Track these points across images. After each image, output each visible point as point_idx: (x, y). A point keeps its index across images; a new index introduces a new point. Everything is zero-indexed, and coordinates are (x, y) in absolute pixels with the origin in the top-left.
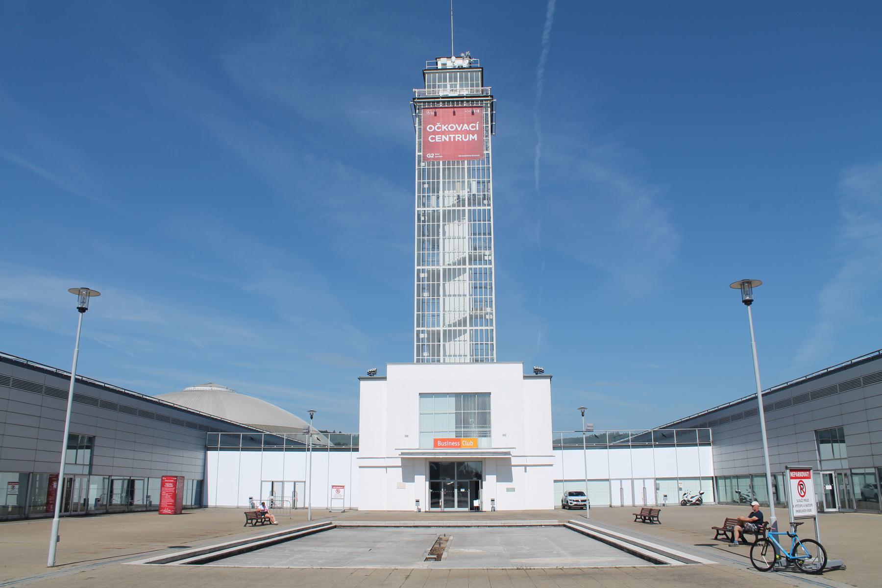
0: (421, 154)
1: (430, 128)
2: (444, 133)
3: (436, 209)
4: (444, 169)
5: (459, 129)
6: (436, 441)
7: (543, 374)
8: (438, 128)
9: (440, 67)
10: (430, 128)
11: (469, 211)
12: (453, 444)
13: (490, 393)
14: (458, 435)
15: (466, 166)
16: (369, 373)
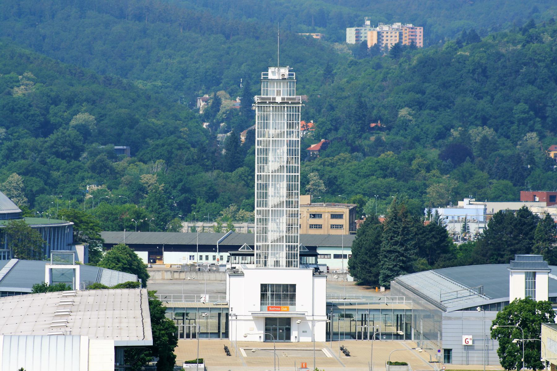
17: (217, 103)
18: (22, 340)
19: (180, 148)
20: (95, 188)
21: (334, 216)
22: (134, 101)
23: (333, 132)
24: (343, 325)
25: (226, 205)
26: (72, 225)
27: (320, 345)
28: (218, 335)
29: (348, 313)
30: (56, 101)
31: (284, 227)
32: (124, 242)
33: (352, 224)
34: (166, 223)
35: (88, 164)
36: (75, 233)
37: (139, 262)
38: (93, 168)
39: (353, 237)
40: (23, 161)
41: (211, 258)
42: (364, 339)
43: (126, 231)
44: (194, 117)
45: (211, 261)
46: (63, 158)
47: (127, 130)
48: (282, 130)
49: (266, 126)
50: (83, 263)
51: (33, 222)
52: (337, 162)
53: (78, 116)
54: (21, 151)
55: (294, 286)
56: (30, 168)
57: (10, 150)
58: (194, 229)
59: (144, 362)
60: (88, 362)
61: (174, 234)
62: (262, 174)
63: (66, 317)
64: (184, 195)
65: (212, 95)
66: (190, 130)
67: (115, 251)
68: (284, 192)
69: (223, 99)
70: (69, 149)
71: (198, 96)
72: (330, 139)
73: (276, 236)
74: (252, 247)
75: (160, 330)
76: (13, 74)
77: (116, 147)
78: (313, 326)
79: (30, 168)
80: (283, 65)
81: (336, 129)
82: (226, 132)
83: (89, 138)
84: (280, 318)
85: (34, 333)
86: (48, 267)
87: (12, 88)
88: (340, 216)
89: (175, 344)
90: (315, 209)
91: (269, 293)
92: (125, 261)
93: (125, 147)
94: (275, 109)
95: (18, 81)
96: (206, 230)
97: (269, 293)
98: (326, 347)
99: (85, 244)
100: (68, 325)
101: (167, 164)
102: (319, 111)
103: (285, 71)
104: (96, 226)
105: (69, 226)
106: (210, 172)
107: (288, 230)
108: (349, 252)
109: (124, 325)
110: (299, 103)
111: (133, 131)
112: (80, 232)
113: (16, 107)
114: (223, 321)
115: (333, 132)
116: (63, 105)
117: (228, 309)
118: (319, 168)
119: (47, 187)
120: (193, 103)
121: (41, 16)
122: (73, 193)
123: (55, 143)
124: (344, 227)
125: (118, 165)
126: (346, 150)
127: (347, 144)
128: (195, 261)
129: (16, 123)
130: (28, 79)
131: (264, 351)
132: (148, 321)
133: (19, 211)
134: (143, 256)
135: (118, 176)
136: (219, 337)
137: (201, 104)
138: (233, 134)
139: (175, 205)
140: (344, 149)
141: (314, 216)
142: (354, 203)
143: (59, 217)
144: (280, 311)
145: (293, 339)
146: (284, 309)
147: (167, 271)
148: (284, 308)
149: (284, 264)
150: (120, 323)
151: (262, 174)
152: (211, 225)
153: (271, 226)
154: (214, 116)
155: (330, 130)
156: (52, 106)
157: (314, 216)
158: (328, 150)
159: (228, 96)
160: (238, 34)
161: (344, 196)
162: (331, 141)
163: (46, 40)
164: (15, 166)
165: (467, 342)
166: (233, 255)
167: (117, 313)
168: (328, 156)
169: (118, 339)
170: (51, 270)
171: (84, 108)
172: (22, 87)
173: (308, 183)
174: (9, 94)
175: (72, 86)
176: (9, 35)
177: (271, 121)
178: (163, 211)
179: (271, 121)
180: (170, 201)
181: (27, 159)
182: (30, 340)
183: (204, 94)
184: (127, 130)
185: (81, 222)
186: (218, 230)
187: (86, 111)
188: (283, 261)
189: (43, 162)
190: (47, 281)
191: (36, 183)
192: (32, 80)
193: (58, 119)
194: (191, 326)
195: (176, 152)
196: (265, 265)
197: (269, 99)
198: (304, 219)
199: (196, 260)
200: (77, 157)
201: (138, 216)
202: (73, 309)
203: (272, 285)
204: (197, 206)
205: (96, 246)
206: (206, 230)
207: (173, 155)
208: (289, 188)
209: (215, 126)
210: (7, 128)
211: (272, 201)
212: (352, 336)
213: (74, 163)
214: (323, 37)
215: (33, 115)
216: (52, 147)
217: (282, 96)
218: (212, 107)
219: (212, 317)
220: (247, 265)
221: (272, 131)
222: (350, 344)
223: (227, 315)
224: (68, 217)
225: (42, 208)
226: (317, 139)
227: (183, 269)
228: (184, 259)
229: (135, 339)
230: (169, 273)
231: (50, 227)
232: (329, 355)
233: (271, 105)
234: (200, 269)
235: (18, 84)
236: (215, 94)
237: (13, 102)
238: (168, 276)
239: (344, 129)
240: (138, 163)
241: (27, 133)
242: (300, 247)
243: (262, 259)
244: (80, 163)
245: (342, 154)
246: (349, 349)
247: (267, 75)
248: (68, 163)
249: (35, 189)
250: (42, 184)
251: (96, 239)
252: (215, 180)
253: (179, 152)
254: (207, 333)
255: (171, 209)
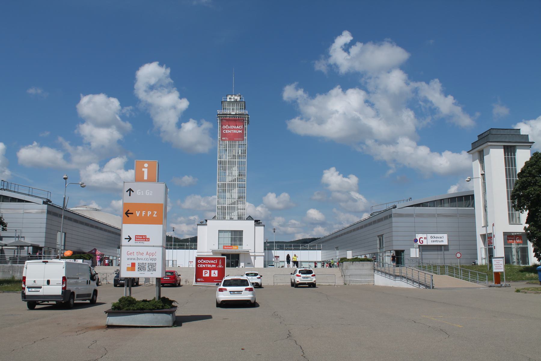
0: (220, 137)
1: (199, 261)
2: (204, 264)
3: (225, 160)
4: (228, 166)
5: (210, 262)
6: (224, 246)
7: (262, 224)
8: (202, 261)
9: (228, 100)
10: (224, 127)
11: (238, 161)
12: (230, 248)
13: (243, 231)
14: (231, 244)
15: (237, 143)
16: (201, 222)
78: (255, 259)
144: (232, 249)
146: (234, 248)
165: (421, 242)
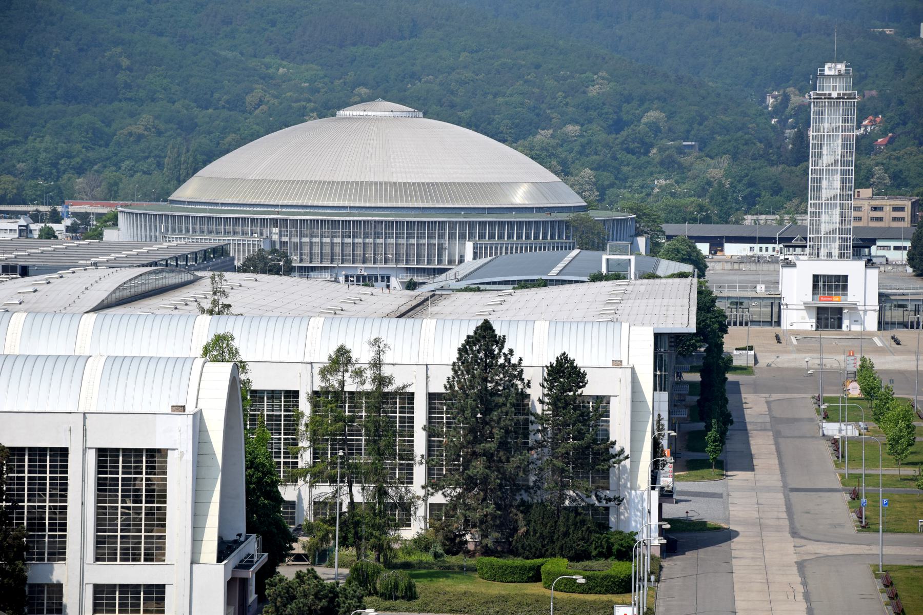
17: (786, 99)
18: (574, 326)
19: (746, 144)
20: (663, 182)
21: (895, 209)
22: (704, 98)
23: (901, 126)
24: (895, 315)
25: (789, 199)
26: (634, 218)
27: (871, 334)
28: (770, 323)
29: (900, 303)
30: (628, 100)
31: (837, 219)
32: (687, 234)
33: (913, 216)
34: (730, 216)
35: (657, 159)
36: (638, 225)
37: (699, 253)
38: (662, 163)
39: (914, 230)
40: (595, 157)
41: (770, 249)
42: (917, 328)
43: (689, 223)
44: (763, 114)
45: (770, 252)
46: (634, 154)
47: (696, 126)
48: (837, 125)
49: (822, 121)
50: (644, 253)
51: (598, 215)
52: (903, 156)
53: (649, 114)
54: (594, 147)
55: (845, 277)
56: (602, 164)
57: (583, 146)
58: (756, 222)
59: (695, 347)
60: (199, 390)
61: (735, 226)
62: (816, 168)
63: (617, 305)
64: (749, 190)
65: (781, 92)
66: (758, 125)
67: (674, 242)
68: (838, 184)
69: (792, 96)
70: (639, 145)
71: (768, 93)
72: (898, 133)
73: (830, 227)
74: (806, 239)
75: (711, 318)
76: (588, 74)
77: (684, 143)
79: (602, 164)
80: (839, 61)
81: (905, 124)
82: (794, 128)
83: (659, 134)
84: (831, 308)
85: (585, 320)
86: (604, 257)
87: (587, 87)
88: (902, 209)
89: (726, 332)
90: (877, 203)
91: (821, 284)
92: (684, 252)
93: (693, 143)
94: (830, 105)
95: (594, 81)
96: (769, 222)
97: (821, 284)
98: (878, 336)
99: (647, 235)
100: (617, 312)
101: (733, 159)
102: (889, 106)
103: (841, 67)
104: (658, 218)
105: (632, 219)
106: (775, 167)
107: (841, 223)
108: (908, 244)
109: (671, 313)
110: (855, 98)
111: (701, 127)
112: (642, 225)
113: (590, 105)
114: (776, 309)
115: (901, 126)
116: (635, 103)
117: (780, 298)
118: (885, 162)
119: (617, 182)
120: (764, 100)
121: (618, 18)
122: (642, 187)
123: (625, 140)
124: (906, 219)
125: (685, 160)
126: (914, 145)
127: (915, 138)
128: (755, 252)
129: (590, 121)
130: (603, 78)
131: (806, 340)
132: (694, 309)
133: (585, 204)
134: (704, 248)
135: (685, 170)
136: (771, 325)
137: (770, 101)
138: (799, 130)
139: (740, 199)
140: (912, 143)
141: (875, 209)
142: (917, 196)
143: (622, 210)
145: (844, 328)
147: (727, 262)
148: (836, 298)
149: (837, 255)
150: (667, 311)
151: (816, 168)
152: (774, 218)
153: (824, 218)
154: (783, 112)
155: (898, 124)
156: (625, 104)
157: (875, 209)
158: (895, 144)
159: (797, 92)
160: (810, 31)
161: (908, 189)
162: (899, 135)
163: (622, 41)
164: (587, 162)
166: (785, 246)
167: (665, 301)
168: (895, 150)
169: (656, 326)
170: (608, 260)
171: (656, 106)
172: (597, 86)
173: (873, 177)
174: (585, 93)
175: (645, 84)
176: (587, 37)
177: (826, 116)
178: (726, 204)
179: (826, 116)
180: (735, 195)
181: (599, 155)
182: (581, 326)
183: (773, 90)
184: (696, 126)
185: (644, 214)
186: (781, 222)
187: (657, 109)
188: (836, 252)
189: (614, 158)
190: (604, 270)
191: (607, 178)
192: (607, 79)
193: (630, 117)
194: (738, 314)
195: (742, 147)
196: (818, 256)
197: (825, 94)
198: (866, 213)
199: (757, 251)
200: (646, 153)
201: (701, 208)
202: (626, 297)
203: (824, 276)
204: (761, 200)
205: (658, 237)
206: (769, 222)
207: (739, 151)
208: (843, 181)
209: (783, 122)
210: (582, 125)
211: (825, 194)
212: (904, 325)
213: (643, 159)
214: (896, 33)
215: (607, 113)
216: (622, 143)
217: (838, 92)
218: (781, 103)
219: (765, 306)
220: (800, 257)
221: (826, 125)
222: (901, 333)
223: (780, 305)
224: (632, 210)
225: (612, 202)
226: (884, 133)
227: (743, 260)
228: (744, 250)
229: (680, 326)
230: (729, 264)
231: (614, 220)
232: (879, 344)
233: (827, 101)
234: (759, 260)
235: (593, 83)
236: (784, 91)
237: (588, 100)
238: (728, 266)
239: (912, 123)
240: (705, 158)
241: (600, 130)
242: (853, 240)
243: (815, 251)
244: (649, 159)
245: (908, 148)
246: (899, 338)
247: (824, 70)
248: (637, 158)
249: (606, 183)
250: (612, 179)
251: (658, 231)
252: (780, 174)
253: (745, 148)
254: (760, 322)
255: (736, 203)
